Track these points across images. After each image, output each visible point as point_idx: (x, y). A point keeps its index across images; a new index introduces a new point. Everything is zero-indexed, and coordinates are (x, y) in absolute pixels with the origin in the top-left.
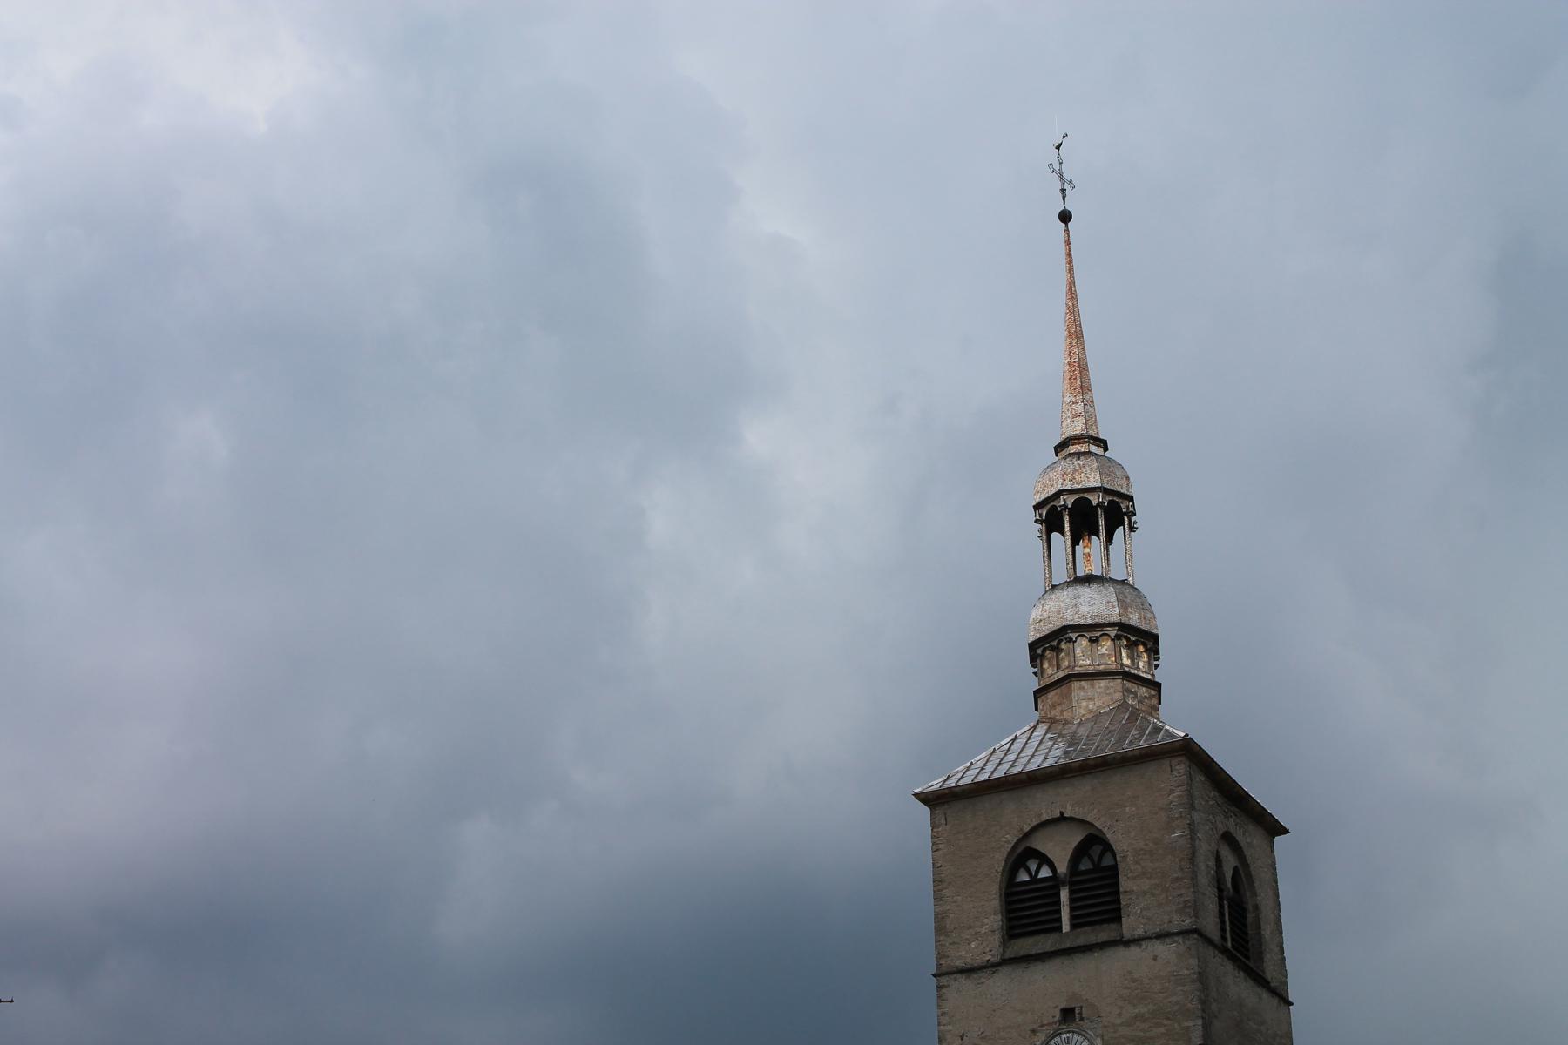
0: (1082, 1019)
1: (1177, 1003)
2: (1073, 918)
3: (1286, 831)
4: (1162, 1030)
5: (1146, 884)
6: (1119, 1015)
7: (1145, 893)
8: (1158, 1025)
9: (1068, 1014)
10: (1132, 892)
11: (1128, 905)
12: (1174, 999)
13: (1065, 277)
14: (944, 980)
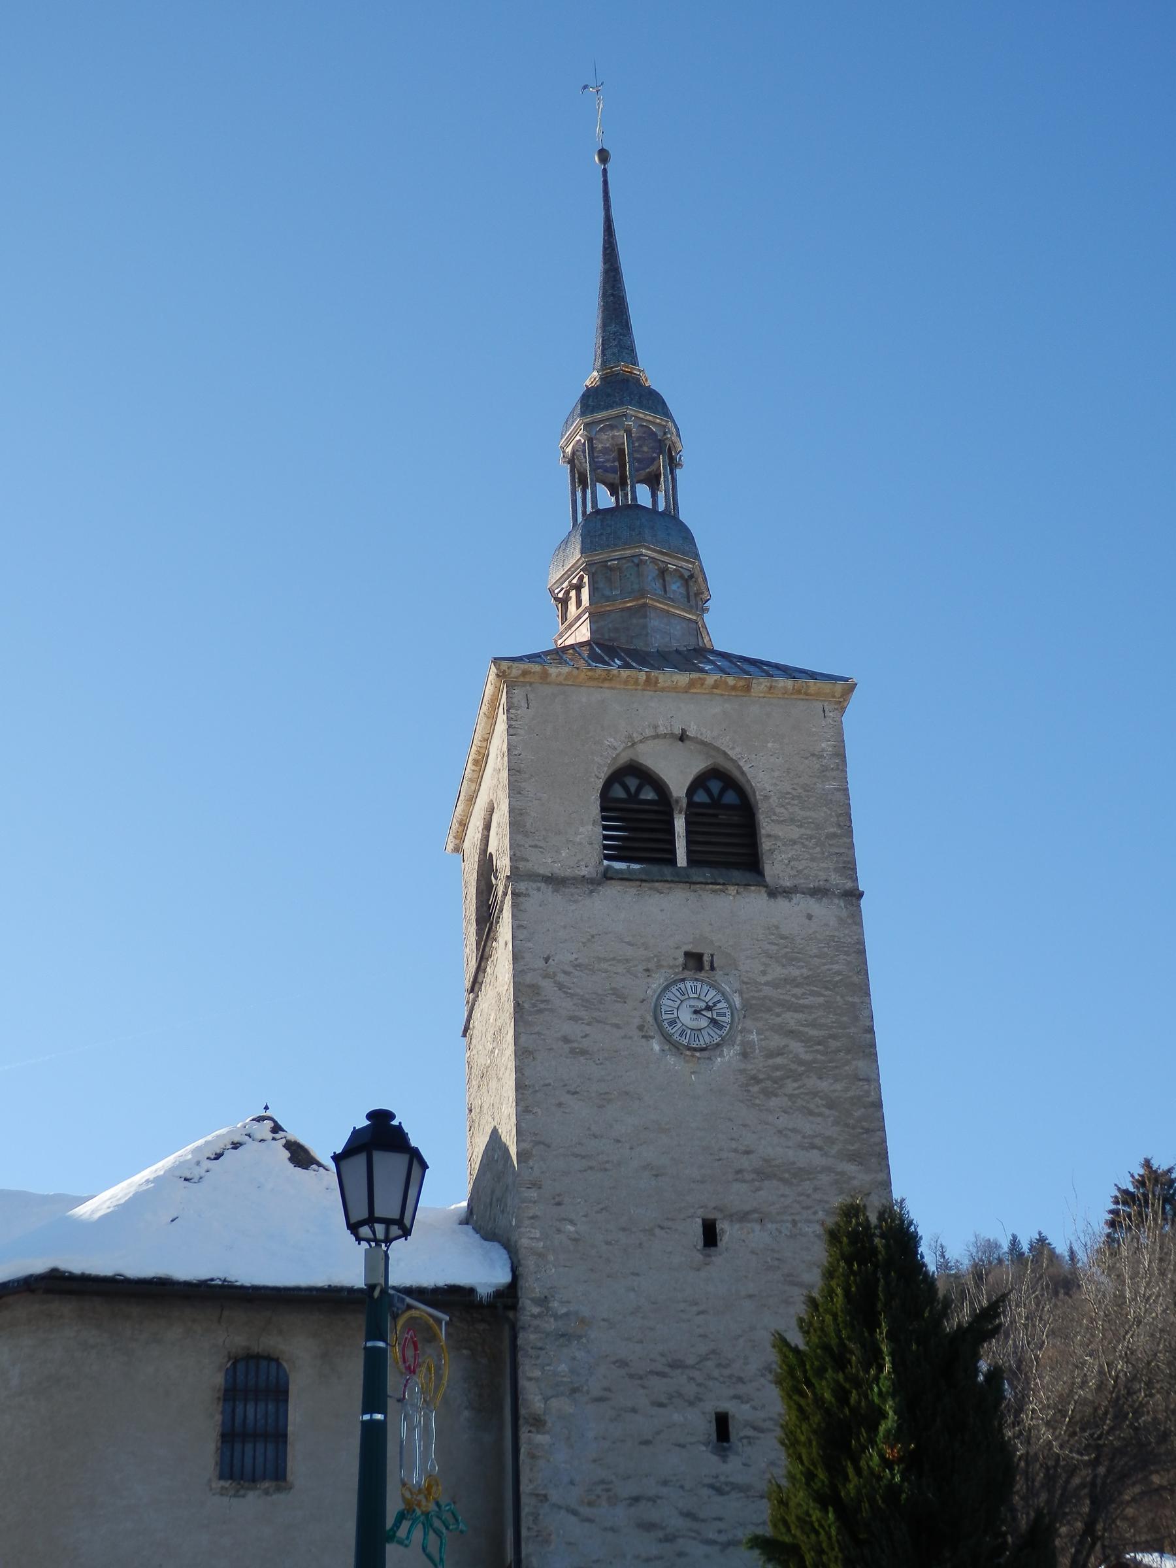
0: (712, 968)
1: (838, 973)
2: (689, 852)
3: (1015, 1237)
4: (821, 1000)
5: (794, 832)
6: (764, 973)
7: (794, 842)
8: (813, 993)
9: (695, 961)
10: (777, 838)
11: (772, 851)
12: (836, 967)
13: (602, 214)
14: (522, 887)
